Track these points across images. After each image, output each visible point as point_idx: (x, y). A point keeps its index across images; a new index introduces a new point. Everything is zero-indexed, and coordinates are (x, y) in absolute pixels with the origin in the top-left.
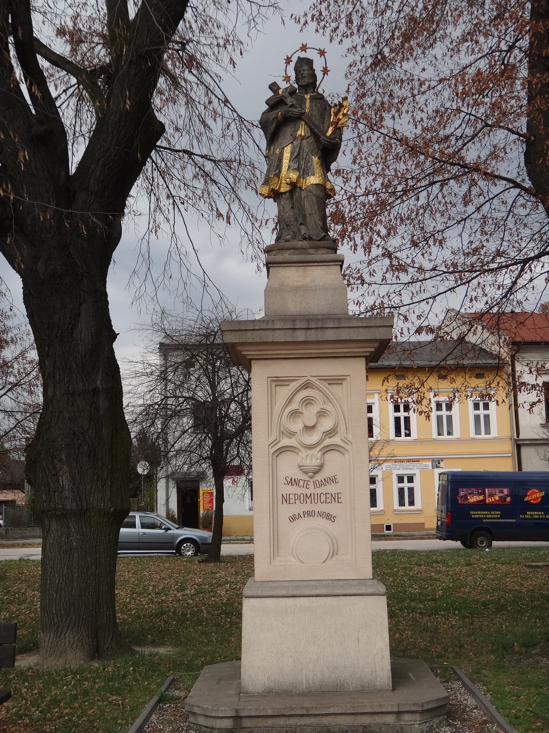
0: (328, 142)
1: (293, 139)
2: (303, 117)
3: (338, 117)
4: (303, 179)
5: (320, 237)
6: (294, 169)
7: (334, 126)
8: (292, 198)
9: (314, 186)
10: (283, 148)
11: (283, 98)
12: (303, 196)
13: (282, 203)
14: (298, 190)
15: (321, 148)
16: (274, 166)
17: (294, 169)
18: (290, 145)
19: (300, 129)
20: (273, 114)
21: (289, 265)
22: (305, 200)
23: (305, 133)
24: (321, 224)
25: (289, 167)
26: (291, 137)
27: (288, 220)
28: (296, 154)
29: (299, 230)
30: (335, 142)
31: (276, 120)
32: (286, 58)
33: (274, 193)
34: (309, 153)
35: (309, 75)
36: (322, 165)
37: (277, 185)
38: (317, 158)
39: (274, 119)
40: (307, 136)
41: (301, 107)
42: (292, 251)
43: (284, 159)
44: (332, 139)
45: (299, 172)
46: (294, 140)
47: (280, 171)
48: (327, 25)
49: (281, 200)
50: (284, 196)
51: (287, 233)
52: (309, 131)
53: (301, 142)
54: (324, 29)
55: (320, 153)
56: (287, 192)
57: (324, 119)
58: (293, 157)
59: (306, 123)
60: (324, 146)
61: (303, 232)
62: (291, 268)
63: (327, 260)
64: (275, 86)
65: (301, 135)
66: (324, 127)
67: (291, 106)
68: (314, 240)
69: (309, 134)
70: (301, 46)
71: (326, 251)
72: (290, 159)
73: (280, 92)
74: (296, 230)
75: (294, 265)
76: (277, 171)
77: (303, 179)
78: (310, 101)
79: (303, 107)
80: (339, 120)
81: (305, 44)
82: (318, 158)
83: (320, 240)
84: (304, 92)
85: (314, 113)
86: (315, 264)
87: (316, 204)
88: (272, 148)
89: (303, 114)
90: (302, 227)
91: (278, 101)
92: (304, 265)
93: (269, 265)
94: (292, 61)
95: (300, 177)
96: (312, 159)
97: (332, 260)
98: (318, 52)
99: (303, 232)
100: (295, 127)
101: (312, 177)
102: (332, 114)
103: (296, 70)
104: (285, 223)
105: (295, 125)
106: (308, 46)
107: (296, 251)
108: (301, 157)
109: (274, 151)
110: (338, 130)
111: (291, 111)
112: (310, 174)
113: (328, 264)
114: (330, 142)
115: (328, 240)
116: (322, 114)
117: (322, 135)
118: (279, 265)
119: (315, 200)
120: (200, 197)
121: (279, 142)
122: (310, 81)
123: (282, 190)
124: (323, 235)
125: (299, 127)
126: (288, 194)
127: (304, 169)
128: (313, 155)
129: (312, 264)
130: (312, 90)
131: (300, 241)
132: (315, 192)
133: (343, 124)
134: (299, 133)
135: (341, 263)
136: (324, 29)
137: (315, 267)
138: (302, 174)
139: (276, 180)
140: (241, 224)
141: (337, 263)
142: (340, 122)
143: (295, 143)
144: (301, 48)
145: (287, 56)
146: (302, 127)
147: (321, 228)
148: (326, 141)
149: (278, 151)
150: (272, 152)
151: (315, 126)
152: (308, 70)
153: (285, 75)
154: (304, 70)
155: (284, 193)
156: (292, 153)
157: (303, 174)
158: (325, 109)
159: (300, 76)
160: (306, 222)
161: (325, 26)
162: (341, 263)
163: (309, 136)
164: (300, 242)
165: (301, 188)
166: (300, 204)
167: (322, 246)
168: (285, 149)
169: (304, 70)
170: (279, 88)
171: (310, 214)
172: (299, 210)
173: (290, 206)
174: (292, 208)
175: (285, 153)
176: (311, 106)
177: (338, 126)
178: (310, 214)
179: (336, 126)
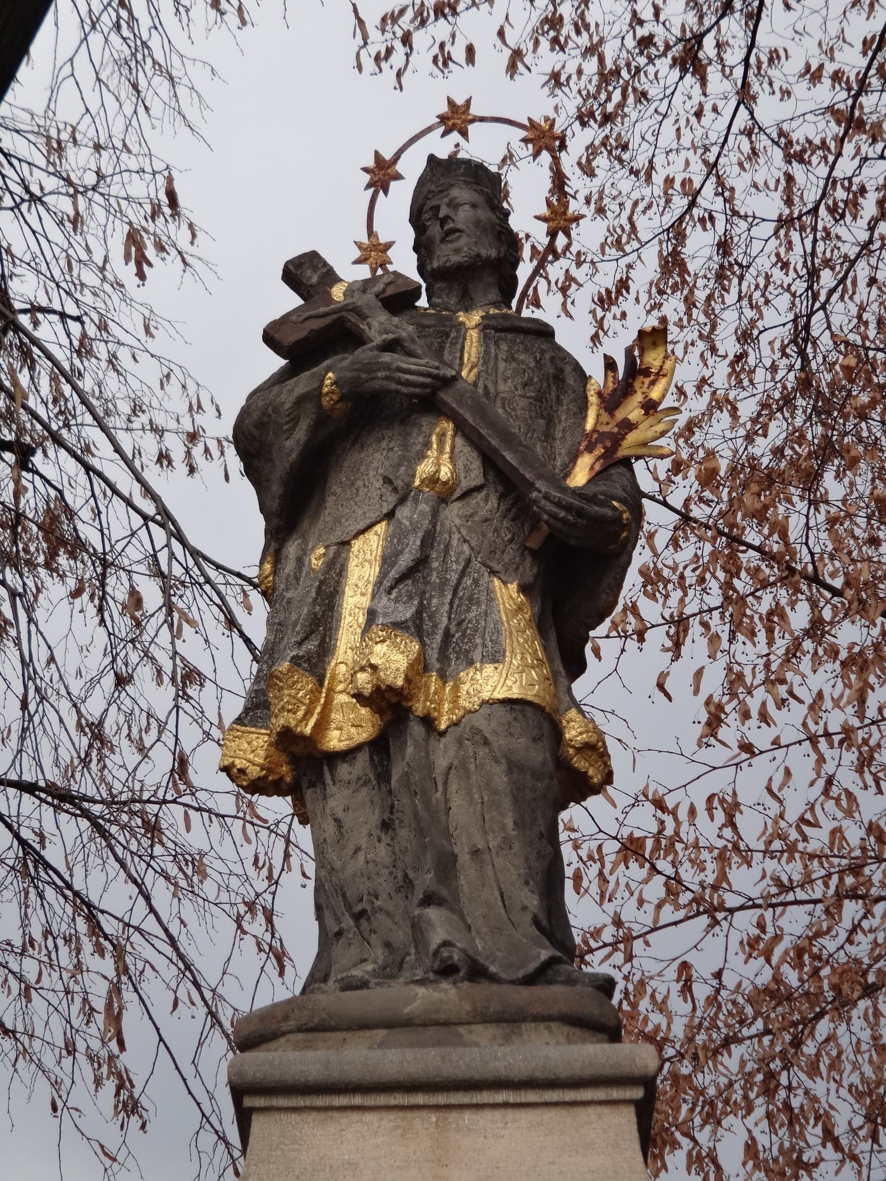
0: (568, 508)
1: (392, 499)
2: (447, 397)
3: (620, 415)
4: (443, 677)
5: (532, 967)
6: (398, 625)
7: (599, 450)
8: (383, 777)
9: (501, 711)
10: (345, 544)
11: (353, 318)
12: (441, 763)
13: (331, 803)
14: (416, 730)
15: (534, 543)
16: (295, 624)
17: (398, 625)
18: (381, 528)
19: (432, 453)
20: (301, 384)
21: (357, 1100)
22: (453, 787)
23: (454, 471)
24: (533, 902)
25: (371, 615)
26: (387, 490)
27: (364, 886)
28: (405, 560)
29: (418, 928)
30: (609, 512)
31: (309, 407)
32: (371, 163)
33: (294, 760)
34: (476, 565)
35: (477, 224)
36: (541, 626)
37: (308, 713)
38: (513, 587)
39: (301, 401)
40: (465, 484)
41: (438, 354)
42: (381, 1033)
43: (348, 591)
44: (592, 499)
45: (423, 644)
46: (402, 501)
47: (326, 650)
48: (579, 274)
49: (331, 789)
50: (343, 770)
51: (354, 952)
52: (476, 465)
53: (435, 514)
54: (564, 290)
55: (529, 570)
56: (359, 748)
57: (550, 422)
58: (394, 574)
59: (461, 427)
60: (550, 539)
61: (436, 938)
62: (368, 1117)
63: (563, 1073)
64: (315, 269)
65: (433, 480)
66: (552, 457)
67: (392, 346)
68: (494, 979)
69: (475, 477)
70: (444, 108)
72: (378, 584)
73: (338, 293)
74: (400, 935)
75: (382, 1100)
76: (311, 645)
77: (443, 677)
78: (485, 338)
79: (447, 357)
80: (628, 426)
81: (460, 101)
82: (524, 589)
83: (530, 980)
84: (453, 301)
85: (502, 387)
86: (501, 1097)
87: (507, 803)
88: (292, 549)
89: (449, 382)
90: (432, 913)
91: (328, 327)
92: (441, 1099)
93: (248, 1102)
94: (398, 177)
95: (426, 669)
96: (490, 592)
97: (588, 1072)
98: (523, 134)
99: (436, 938)
100: (405, 446)
101: (489, 669)
102: (593, 399)
103: (417, 218)
104: (349, 906)
105: (406, 435)
106: (474, 111)
107: (399, 1035)
108: (434, 578)
109: (300, 561)
110: (622, 469)
111: (387, 367)
112: (477, 655)
113: (570, 1095)
114: (580, 513)
115: (570, 981)
116: (540, 399)
117: (540, 477)
118: (300, 1102)
119: (500, 778)
120: (28, 988)
121: (327, 515)
122: (484, 252)
123: (335, 740)
124: (545, 954)
125: (427, 445)
126: (363, 758)
127: (447, 635)
128: (493, 572)
129: (485, 1097)
130: (494, 295)
131: (421, 982)
132: (499, 742)
133: (645, 444)
134: (425, 468)
135: (638, 1093)
136: (564, 290)
137: (498, 1114)
138: (433, 655)
139: (304, 685)
140: (188, 1071)
141: (616, 1094)
142: (632, 437)
143: (404, 513)
144: (443, 119)
145: (377, 155)
146: (441, 450)
147: (536, 922)
148: (558, 504)
149: (317, 559)
150: (289, 567)
151: (508, 438)
152: (474, 206)
153: (364, 239)
154: (454, 205)
156: (388, 560)
157: (443, 657)
158: (559, 379)
159: (435, 230)
160: (455, 893)
161: (569, 278)
162: (638, 1093)
163: (478, 489)
164: (421, 991)
165: (428, 722)
166: (427, 803)
167: (538, 1009)
168: (357, 545)
169: (454, 205)
170: (330, 277)
171: (475, 853)
172: (421, 832)
173: (374, 818)
174: (386, 826)
175: (352, 564)
176: (485, 358)
177: (622, 453)
178: (475, 853)
179: (610, 452)
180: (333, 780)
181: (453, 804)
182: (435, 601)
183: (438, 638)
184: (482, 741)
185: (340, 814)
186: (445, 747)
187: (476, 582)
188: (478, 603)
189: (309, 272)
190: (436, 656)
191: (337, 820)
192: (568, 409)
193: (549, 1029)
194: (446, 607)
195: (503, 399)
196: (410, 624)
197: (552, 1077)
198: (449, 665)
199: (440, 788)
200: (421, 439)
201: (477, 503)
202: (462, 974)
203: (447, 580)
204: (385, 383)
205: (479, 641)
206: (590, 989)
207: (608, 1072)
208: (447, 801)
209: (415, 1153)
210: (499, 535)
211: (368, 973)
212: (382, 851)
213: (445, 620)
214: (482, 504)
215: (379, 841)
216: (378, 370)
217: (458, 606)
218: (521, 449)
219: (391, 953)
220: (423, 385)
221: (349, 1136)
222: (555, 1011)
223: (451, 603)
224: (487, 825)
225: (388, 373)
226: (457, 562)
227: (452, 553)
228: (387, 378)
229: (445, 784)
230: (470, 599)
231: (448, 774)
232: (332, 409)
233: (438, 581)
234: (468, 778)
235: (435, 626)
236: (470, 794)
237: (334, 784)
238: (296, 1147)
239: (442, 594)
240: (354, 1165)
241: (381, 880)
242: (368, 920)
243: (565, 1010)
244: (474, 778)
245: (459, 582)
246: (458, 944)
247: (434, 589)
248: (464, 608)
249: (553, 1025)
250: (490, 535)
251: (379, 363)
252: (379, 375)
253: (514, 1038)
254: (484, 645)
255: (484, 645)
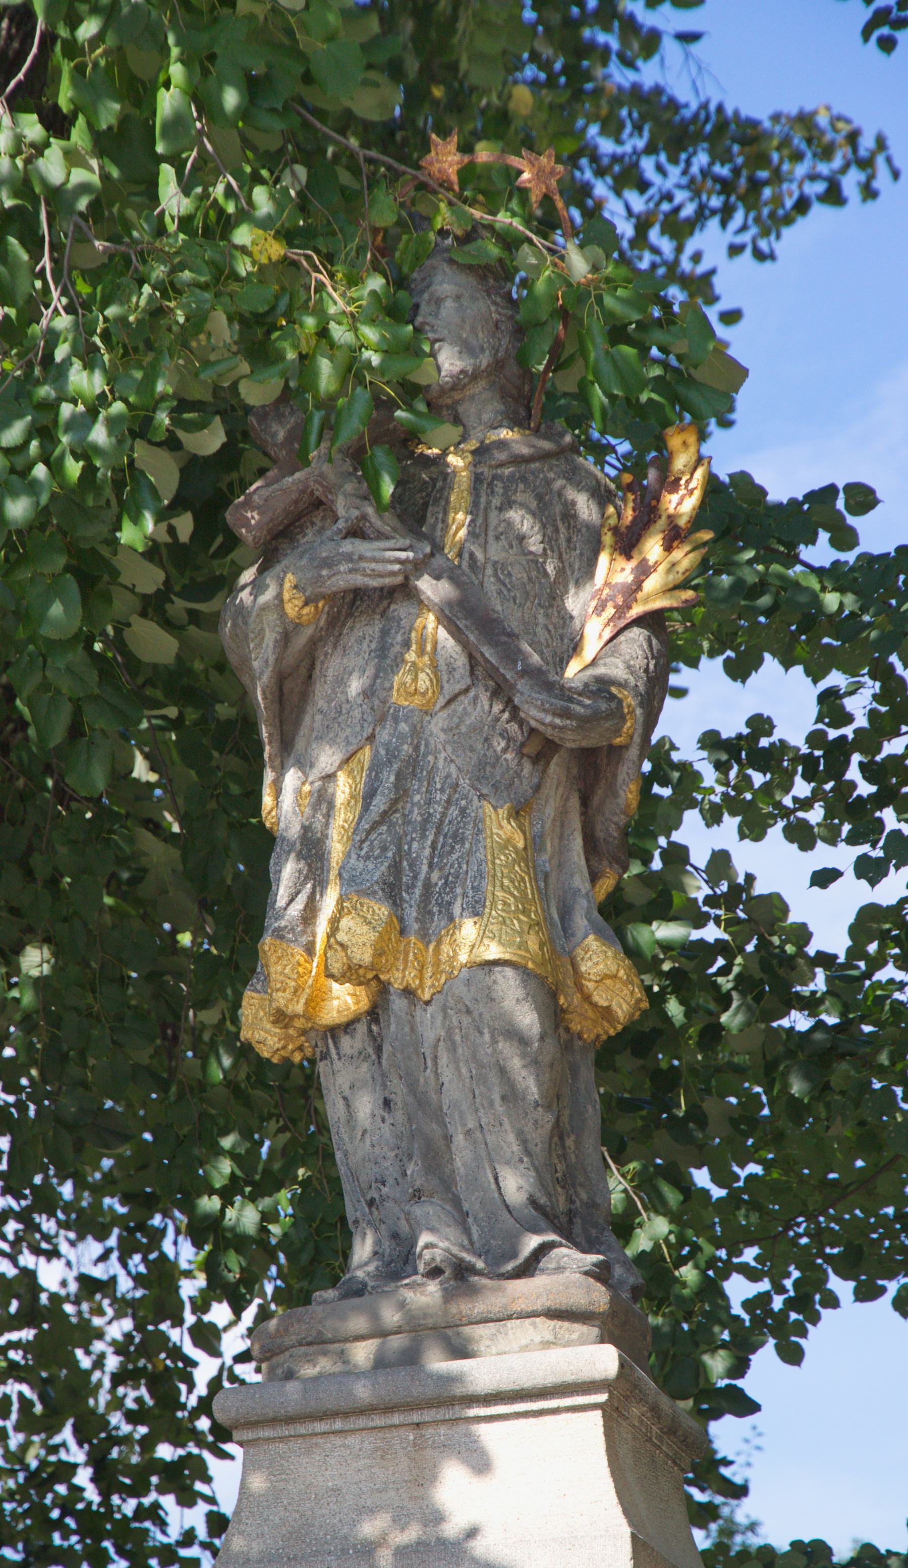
4: (424, 936)
14: (398, 1004)
21: (338, 1425)
28: (380, 803)
50: (346, 1042)
71: (545, 1328)
96: (478, 822)
138: (411, 913)
155: (348, 1027)
180: (338, 1054)
181: (445, 1079)
182: (415, 845)
183: (418, 892)
184: (464, 1009)
185: (347, 1093)
186: (432, 1017)
187: (463, 811)
188: (463, 841)
189: (275, 427)
190: (414, 914)
191: (345, 1099)
192: (582, 554)
193: (534, 1325)
194: (427, 852)
195: (495, 563)
196: (376, 888)
197: (518, 1388)
198: (433, 921)
199: (429, 1063)
200: (399, 638)
201: (465, 709)
202: (446, 1274)
203: (430, 815)
204: (349, 577)
205: (459, 890)
206: (578, 1275)
207: (569, 1378)
208: (437, 1074)
209: (394, 1474)
210: (490, 746)
211: (368, 1274)
212: (386, 1129)
213: (425, 868)
214: (470, 709)
215: (383, 1121)
216: (340, 563)
217: (443, 846)
218: (504, 639)
219: (398, 1245)
220: (393, 574)
221: (333, 1462)
222: (538, 1306)
223: (433, 846)
224: (478, 1100)
225: (350, 565)
226: (442, 790)
227: (437, 779)
228: (350, 571)
229: (435, 1058)
230: (455, 836)
231: (436, 1046)
232: (300, 616)
233: (419, 818)
234: (455, 1050)
235: (415, 877)
236: (458, 1069)
237: (340, 1059)
238: (283, 1477)
239: (423, 836)
240: (336, 1490)
241: (387, 1164)
242: (377, 1209)
243: (548, 1304)
244: (460, 1051)
245: (444, 815)
246: (441, 1244)
247: (414, 831)
248: (448, 848)
249: (538, 1320)
250: (479, 746)
251: (339, 554)
252: (342, 569)
253: (500, 1337)
254: (465, 895)
255: (465, 895)
